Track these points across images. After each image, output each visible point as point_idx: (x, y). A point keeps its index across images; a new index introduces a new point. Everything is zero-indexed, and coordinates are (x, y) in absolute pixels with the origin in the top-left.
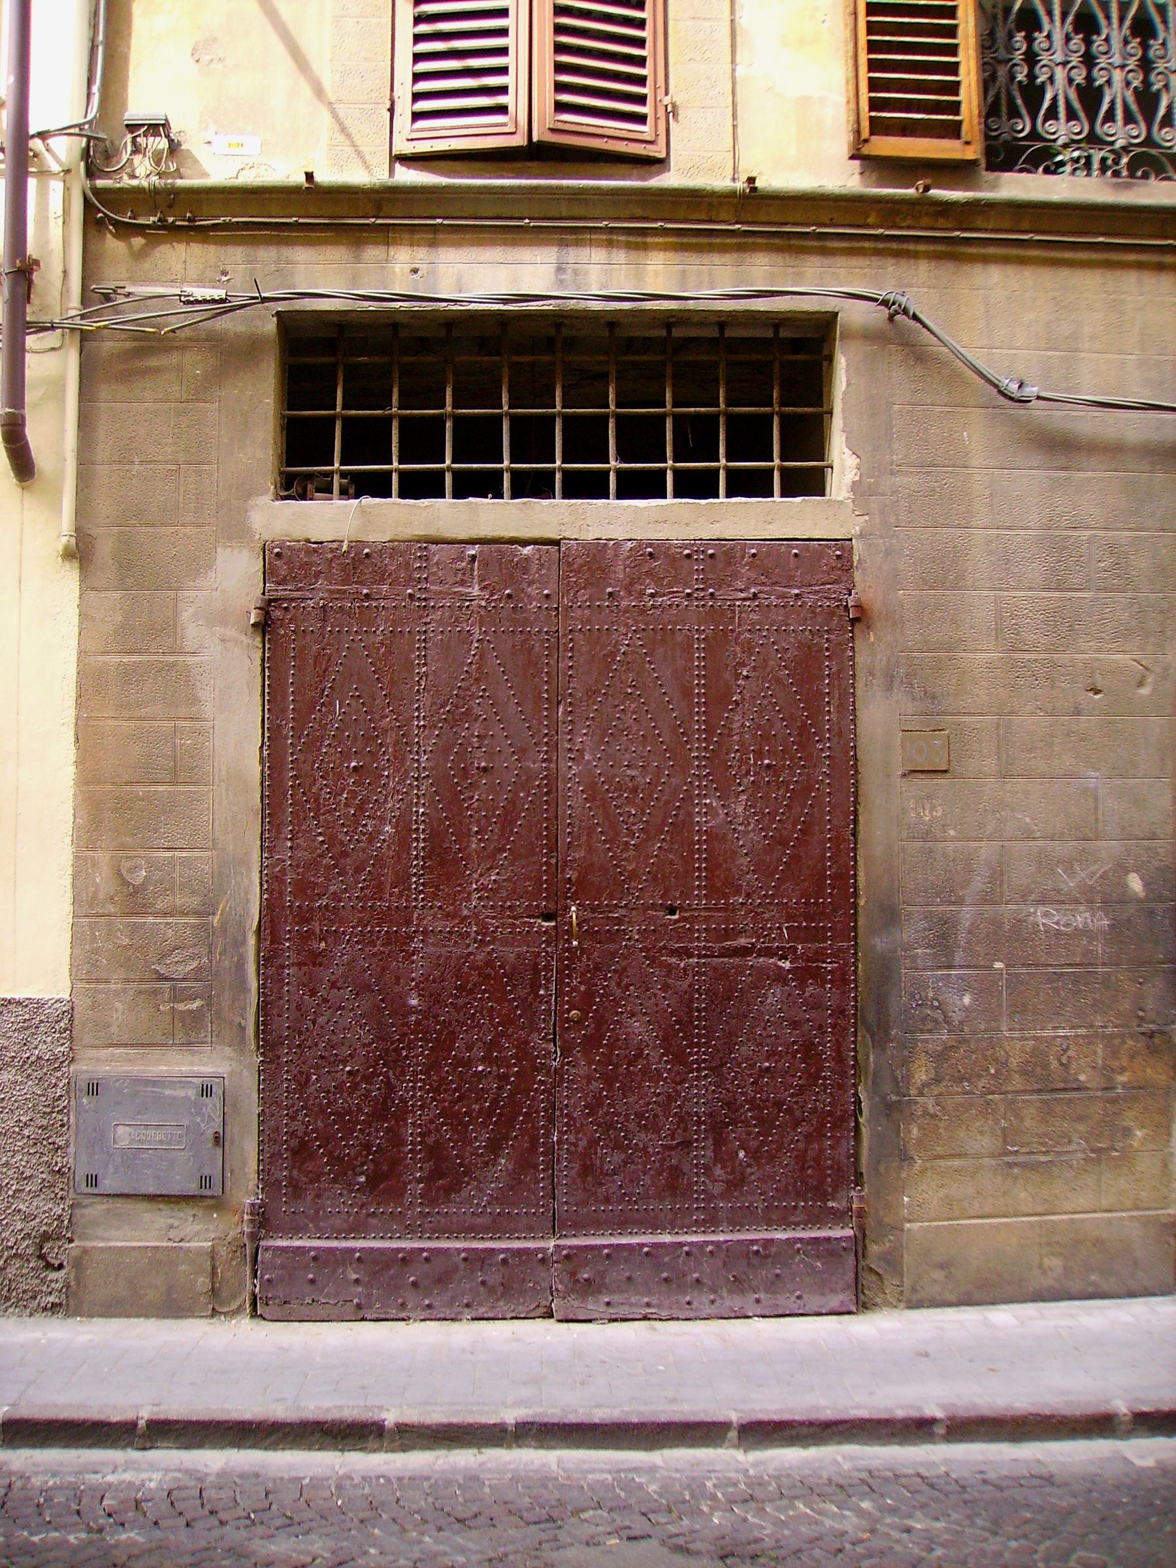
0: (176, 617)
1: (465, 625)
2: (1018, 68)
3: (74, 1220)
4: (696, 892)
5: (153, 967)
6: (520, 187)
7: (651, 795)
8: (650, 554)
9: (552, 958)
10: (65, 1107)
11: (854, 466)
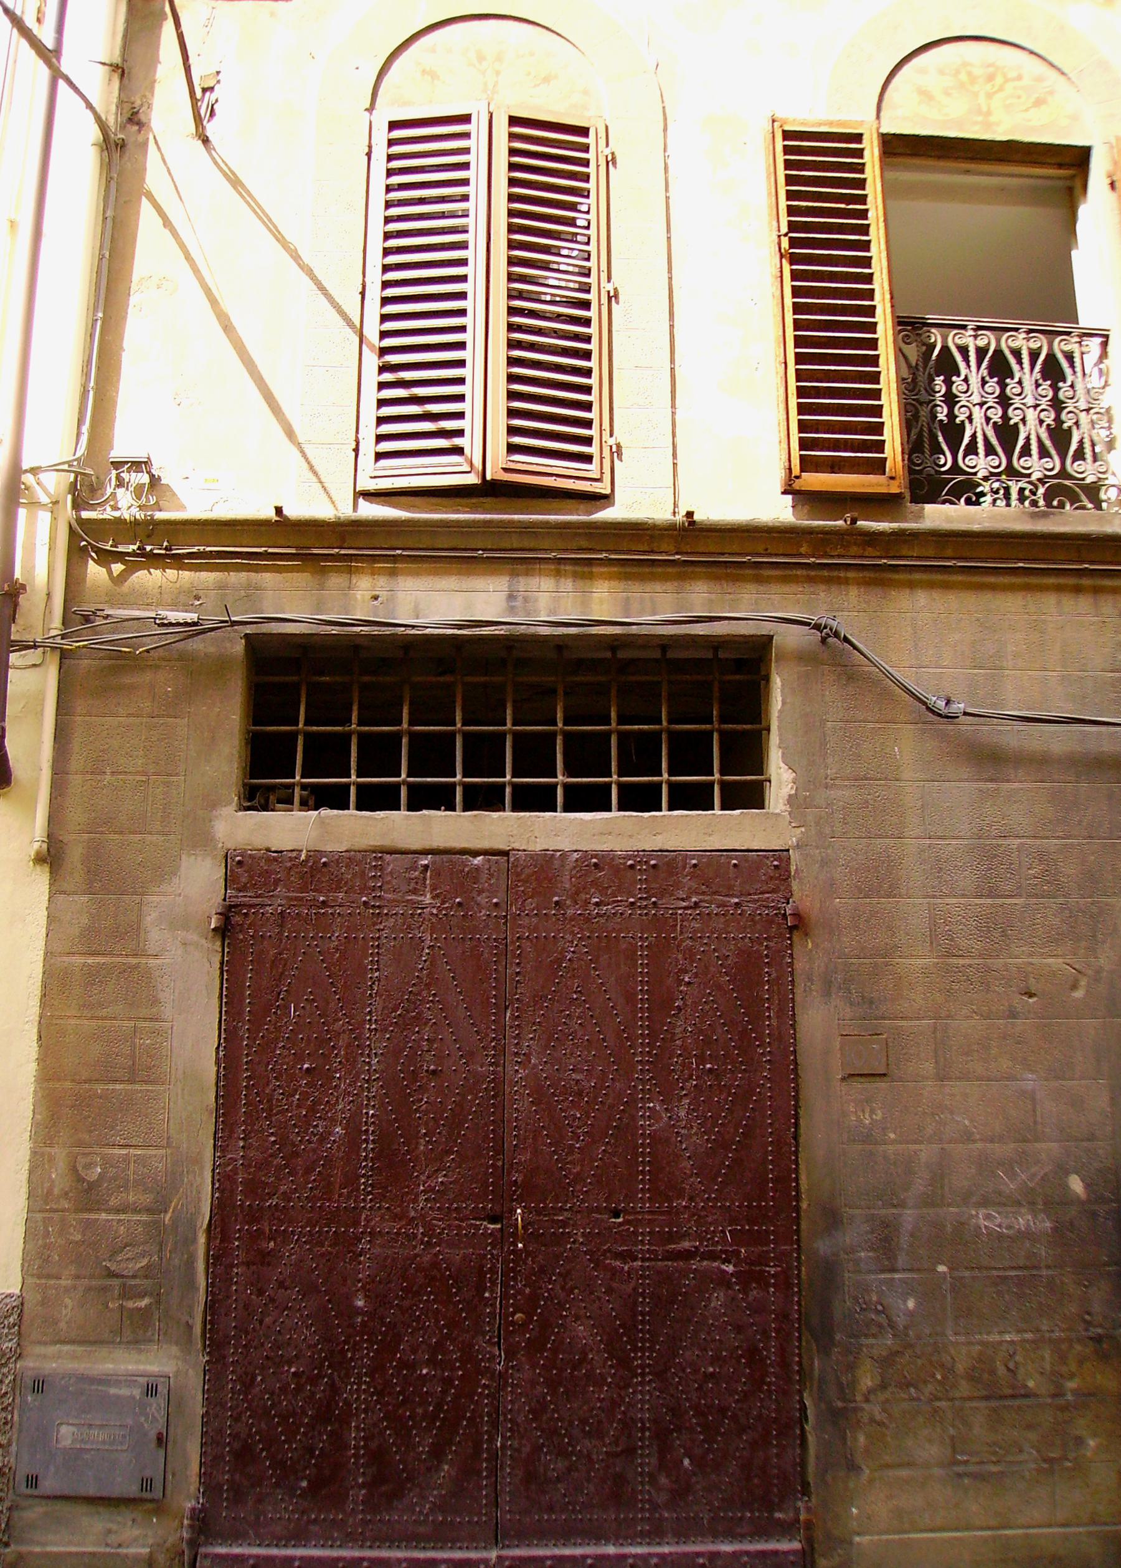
0: (139, 922)
1: (416, 932)
2: (939, 409)
3: (11, 1523)
4: (640, 1196)
5: (104, 1263)
6: (474, 521)
7: (596, 1098)
8: (596, 865)
9: (498, 1260)
10: (9, 1404)
11: (790, 780)
